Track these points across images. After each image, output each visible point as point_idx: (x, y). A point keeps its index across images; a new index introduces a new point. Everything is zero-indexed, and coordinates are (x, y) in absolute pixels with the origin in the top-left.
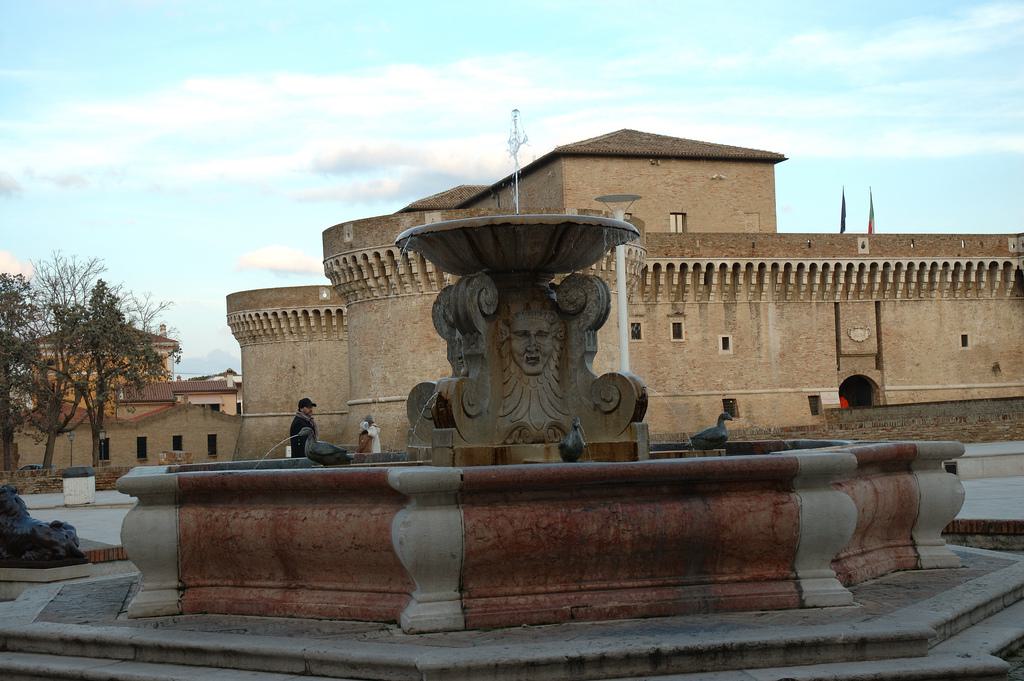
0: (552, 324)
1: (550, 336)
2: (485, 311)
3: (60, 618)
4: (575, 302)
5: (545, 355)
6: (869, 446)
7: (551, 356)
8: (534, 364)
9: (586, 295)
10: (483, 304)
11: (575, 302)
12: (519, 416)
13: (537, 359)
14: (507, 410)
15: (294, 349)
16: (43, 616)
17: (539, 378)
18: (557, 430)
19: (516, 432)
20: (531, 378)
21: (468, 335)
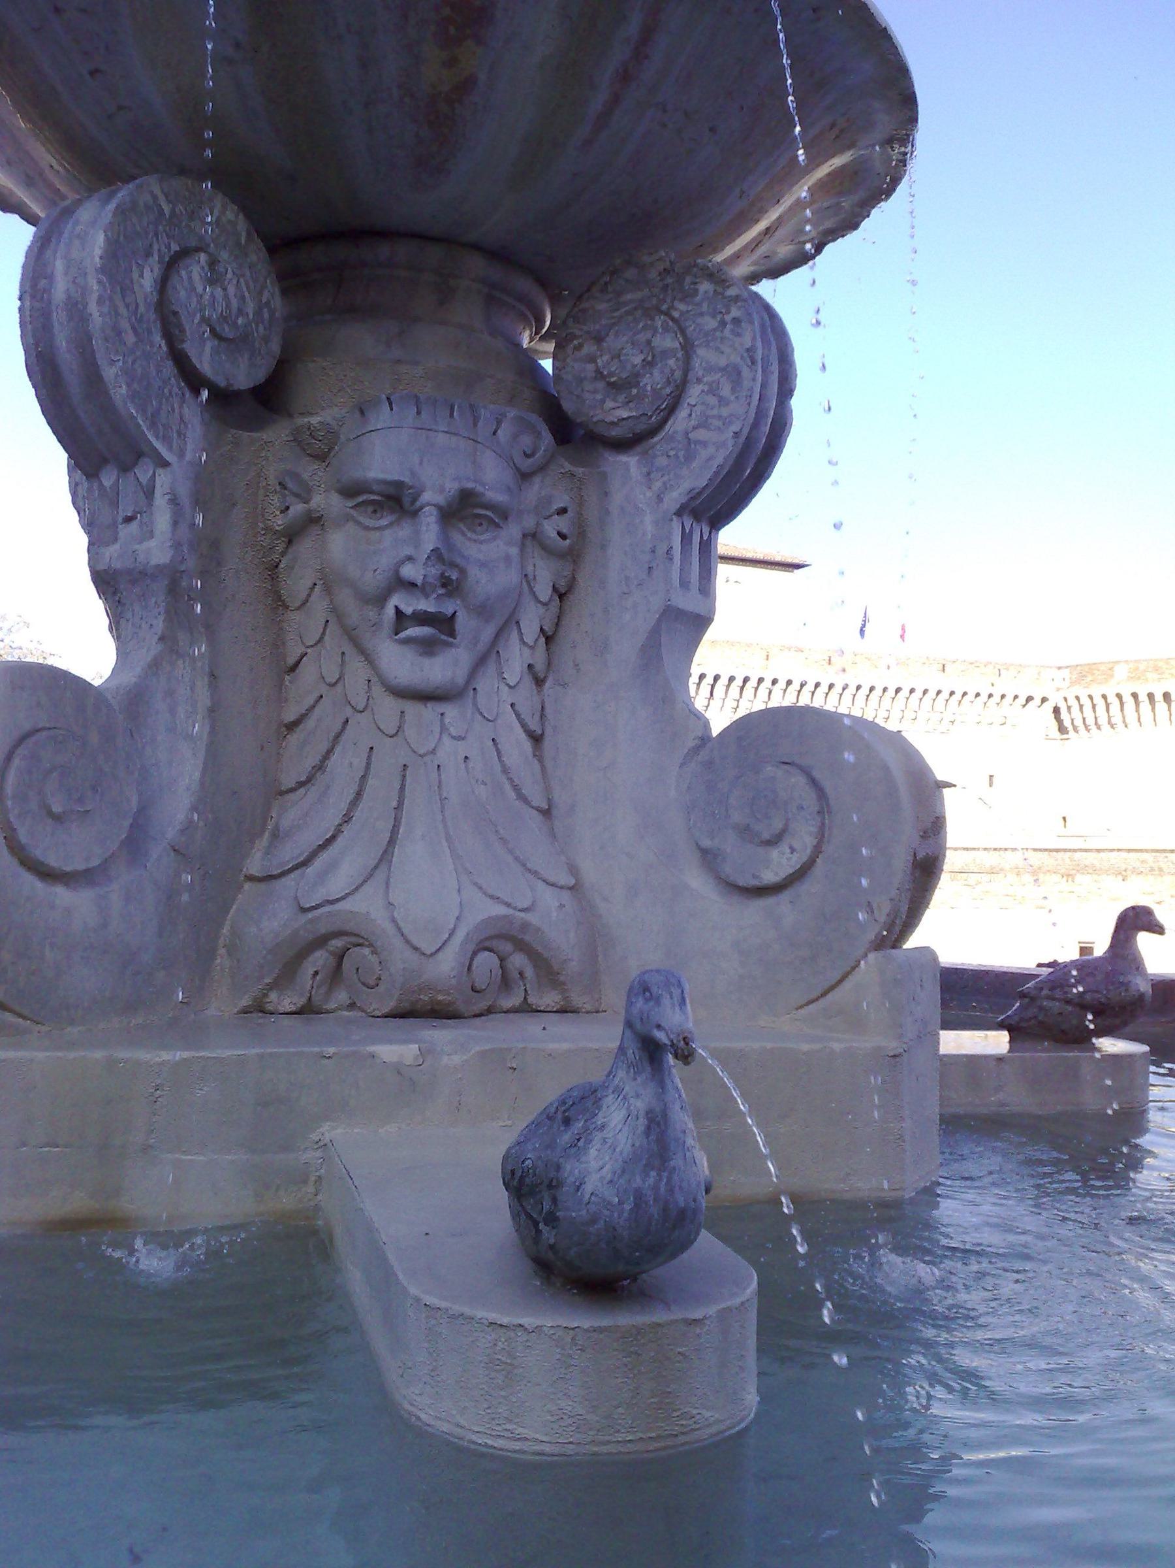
0: (525, 476)
1: (513, 530)
2: (204, 360)
3: (725, 1066)
4: (633, 380)
5: (483, 611)
6: (967, 1414)
7: (512, 621)
8: (428, 647)
9: (688, 348)
10: (191, 325)
11: (633, 380)
12: (336, 885)
13: (445, 624)
14: (290, 852)
15: (427, 438)
16: (726, 1058)
17: (451, 711)
18: (518, 961)
19: (320, 959)
20: (413, 709)
21: (108, 478)
